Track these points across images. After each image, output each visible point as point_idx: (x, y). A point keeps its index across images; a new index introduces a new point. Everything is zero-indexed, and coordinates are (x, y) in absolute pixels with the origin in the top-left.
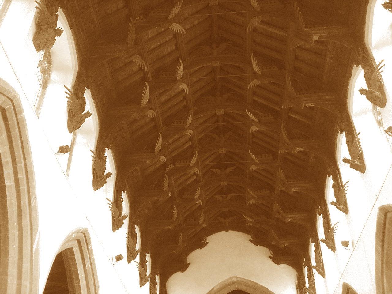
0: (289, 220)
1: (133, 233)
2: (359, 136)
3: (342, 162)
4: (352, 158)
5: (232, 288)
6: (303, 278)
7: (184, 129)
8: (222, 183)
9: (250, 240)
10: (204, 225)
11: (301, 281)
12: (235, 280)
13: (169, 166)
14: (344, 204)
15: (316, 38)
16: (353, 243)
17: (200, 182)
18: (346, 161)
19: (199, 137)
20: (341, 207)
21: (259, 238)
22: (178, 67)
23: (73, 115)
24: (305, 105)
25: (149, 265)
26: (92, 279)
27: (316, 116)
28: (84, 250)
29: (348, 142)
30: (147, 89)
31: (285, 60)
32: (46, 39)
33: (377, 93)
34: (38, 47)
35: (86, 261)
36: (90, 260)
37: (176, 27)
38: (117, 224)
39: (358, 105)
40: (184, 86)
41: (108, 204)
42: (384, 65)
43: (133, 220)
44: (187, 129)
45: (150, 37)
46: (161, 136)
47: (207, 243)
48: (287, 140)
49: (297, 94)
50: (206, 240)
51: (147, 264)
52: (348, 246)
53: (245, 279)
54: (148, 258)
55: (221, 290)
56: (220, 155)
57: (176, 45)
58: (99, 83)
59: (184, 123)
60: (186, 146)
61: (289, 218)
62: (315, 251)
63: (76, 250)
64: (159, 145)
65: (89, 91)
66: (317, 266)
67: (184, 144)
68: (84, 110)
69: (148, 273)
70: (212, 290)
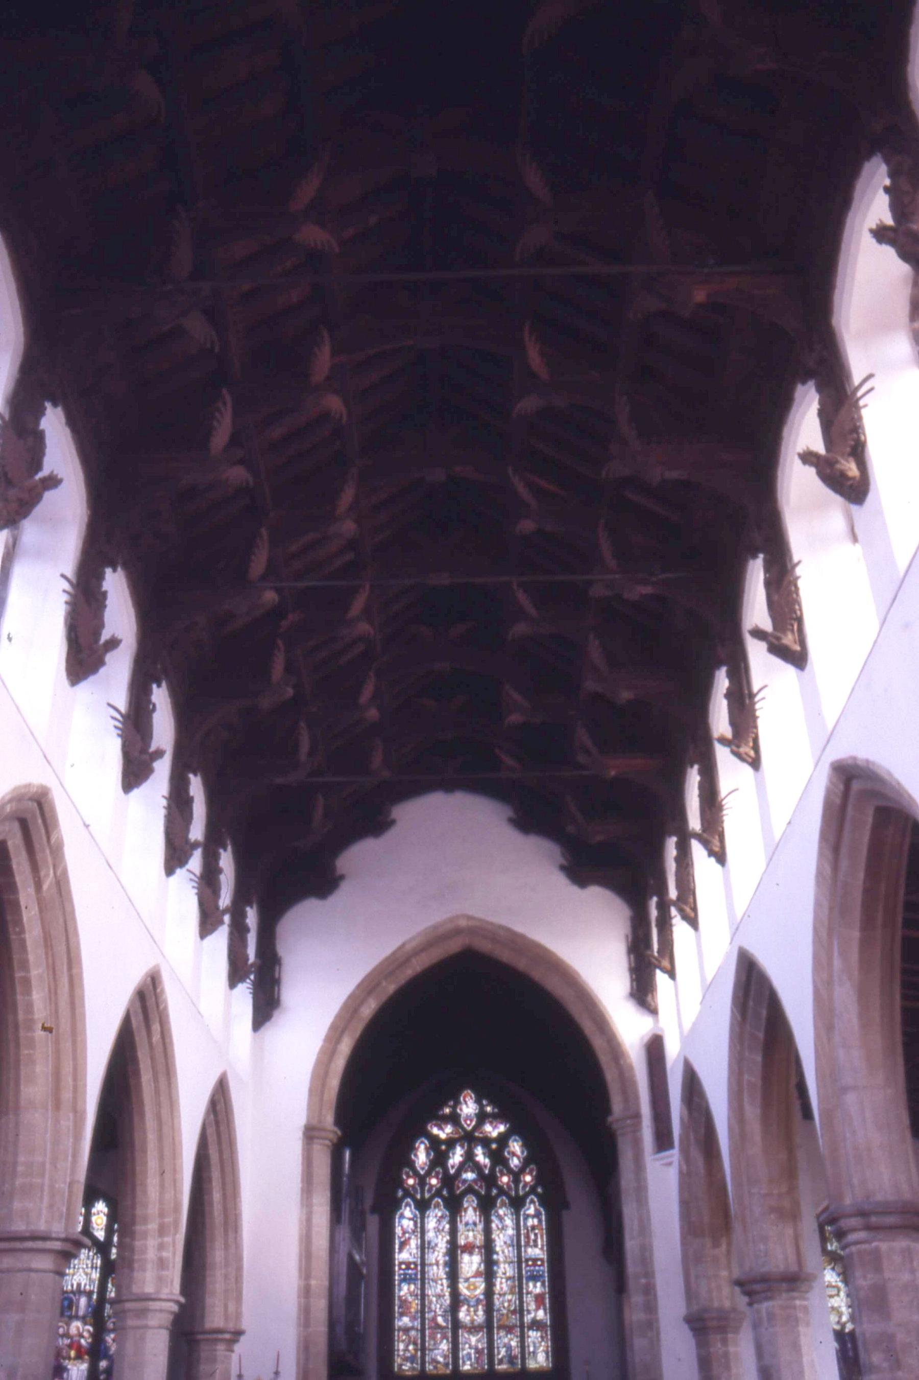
0: (613, 773)
3: (798, 462)
4: (775, 628)
5: (454, 946)
10: (386, 774)
12: (463, 923)
13: (290, 616)
18: (758, 634)
29: (768, 584)
35: (42, 873)
36: (55, 873)
37: (313, 235)
38: (135, 772)
39: (798, 487)
40: (334, 403)
41: (113, 718)
42: (872, 389)
50: (389, 812)
51: (222, 877)
54: (226, 861)
62: (678, 860)
64: (259, 564)
65: (59, 410)
66: (679, 898)
68: (39, 466)
69: (225, 899)
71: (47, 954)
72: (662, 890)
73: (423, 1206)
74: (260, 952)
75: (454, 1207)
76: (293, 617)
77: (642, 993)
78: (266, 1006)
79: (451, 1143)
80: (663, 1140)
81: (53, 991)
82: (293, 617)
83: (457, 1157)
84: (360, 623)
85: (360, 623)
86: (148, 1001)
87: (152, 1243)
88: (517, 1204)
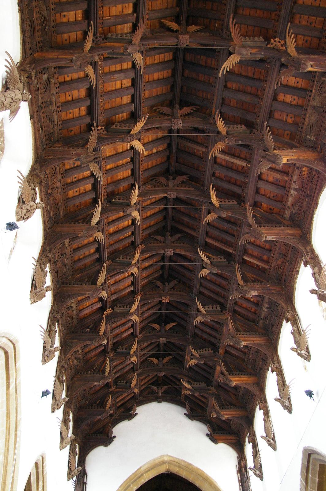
0: (235, 384)
1: (61, 378)
5: (162, 470)
6: (245, 460)
7: (129, 265)
9: (185, 414)
11: (242, 464)
12: (166, 459)
13: (108, 310)
14: (306, 350)
15: (284, 160)
16: (317, 393)
17: (137, 336)
19: (142, 283)
20: (303, 352)
21: (196, 411)
22: (133, 191)
23: (24, 203)
24: (266, 238)
26: (15, 406)
27: (273, 257)
28: (10, 366)
30: (99, 207)
31: (244, 194)
32: (12, 99)
34: (2, 105)
38: (46, 357)
43: (61, 364)
44: (133, 265)
45: (107, 155)
46: (105, 267)
47: (136, 414)
48: (241, 282)
49: (257, 226)
52: (313, 396)
53: (179, 459)
55: (149, 470)
57: (132, 170)
58: (49, 192)
59: (130, 259)
61: (235, 381)
67: (125, 288)
70: (138, 469)
71: (7, 421)
81: (7, 440)
82: (109, 311)
86: (39, 467)
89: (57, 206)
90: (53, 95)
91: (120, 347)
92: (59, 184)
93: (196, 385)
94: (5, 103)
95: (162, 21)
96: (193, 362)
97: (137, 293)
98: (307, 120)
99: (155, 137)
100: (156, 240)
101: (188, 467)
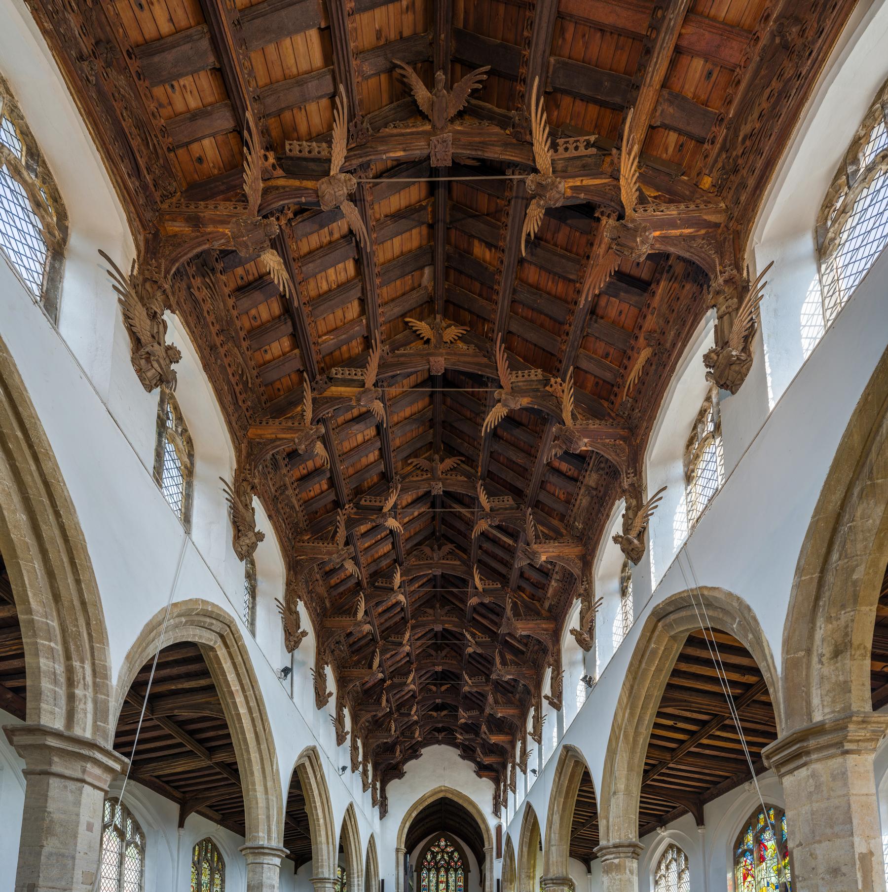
2: (564, 674)
3: (569, 633)
5: (441, 795)
7: (401, 644)
8: (437, 701)
10: (420, 739)
18: (546, 697)
21: (468, 753)
25: (370, 774)
33: (586, 636)
38: (340, 740)
40: (401, 598)
54: (370, 767)
56: (436, 672)
57: (393, 543)
60: (403, 662)
61: (494, 739)
63: (307, 764)
68: (299, 628)
72: (505, 782)
73: (429, 870)
74: (381, 797)
75: (438, 871)
76: (389, 682)
77: (496, 812)
78: (383, 813)
79: (438, 853)
80: (499, 855)
82: (389, 682)
83: (439, 857)
84: (412, 684)
85: (412, 684)
86: (350, 811)
87: (356, 880)
88: (456, 870)
89: (322, 600)
90: (285, 475)
91: (403, 706)
92: (318, 576)
93: (467, 737)
94: (243, 552)
95: (407, 319)
96: (463, 721)
97: (412, 664)
98: (578, 501)
99: (415, 497)
100: (426, 612)
101: (459, 794)
